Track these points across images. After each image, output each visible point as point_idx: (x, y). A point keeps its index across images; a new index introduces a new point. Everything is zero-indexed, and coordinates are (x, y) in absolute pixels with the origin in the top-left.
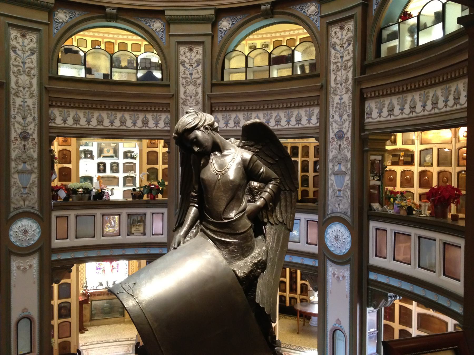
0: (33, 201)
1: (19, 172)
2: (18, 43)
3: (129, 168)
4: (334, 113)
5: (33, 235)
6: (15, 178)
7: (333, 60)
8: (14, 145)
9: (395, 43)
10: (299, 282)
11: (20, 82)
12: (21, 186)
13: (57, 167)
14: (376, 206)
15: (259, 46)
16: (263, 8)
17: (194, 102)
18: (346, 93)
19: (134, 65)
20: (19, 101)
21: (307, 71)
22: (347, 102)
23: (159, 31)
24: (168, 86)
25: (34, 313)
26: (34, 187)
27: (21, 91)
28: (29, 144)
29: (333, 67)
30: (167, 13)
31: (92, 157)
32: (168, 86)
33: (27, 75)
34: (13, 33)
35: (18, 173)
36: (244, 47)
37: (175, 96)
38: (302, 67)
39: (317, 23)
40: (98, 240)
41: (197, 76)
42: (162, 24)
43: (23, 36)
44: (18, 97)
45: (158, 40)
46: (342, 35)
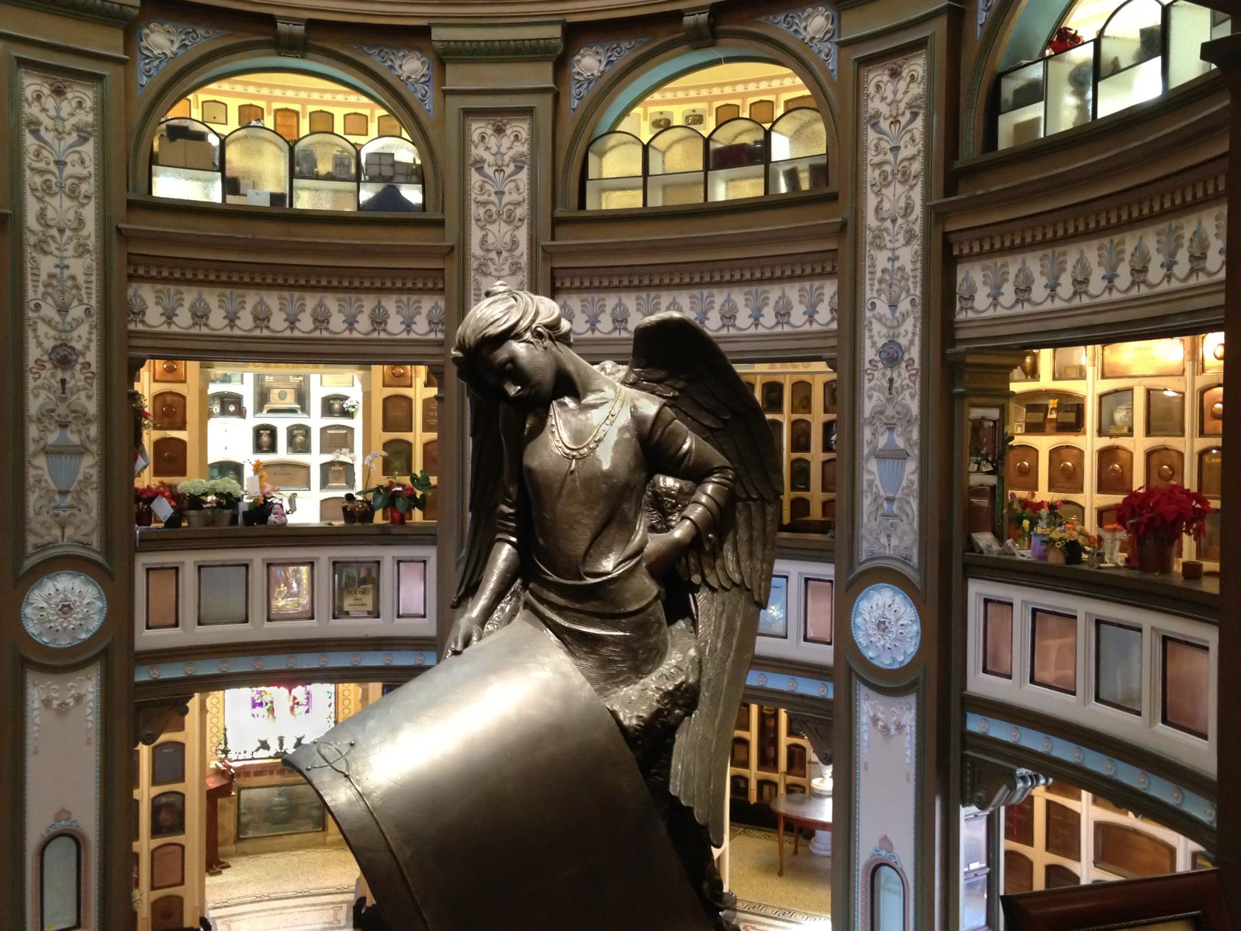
0: (86, 526)
1: (48, 451)
2: (44, 110)
3: (337, 440)
4: (875, 295)
5: (87, 617)
6: (39, 468)
7: (871, 156)
8: (35, 379)
9: (1034, 111)
10: (784, 740)
11: (50, 213)
12: (53, 487)
13: (149, 437)
14: (984, 539)
15: (678, 120)
16: (688, 20)
17: (506, 267)
18: (908, 243)
19: (351, 170)
20: (47, 265)
21: (805, 185)
22: (909, 267)
23: (417, 81)
24: (440, 223)
25: (88, 822)
26: (89, 490)
27: (53, 237)
28: (76, 378)
29: (872, 175)
30: (437, 34)
31: (240, 413)
32: (440, 223)
33: (70, 197)
34: (31, 85)
35: (46, 453)
36: (639, 123)
37: (458, 251)
38: (792, 176)
39: (830, 60)
40: (257, 630)
41: (516, 197)
42: (423, 63)
43: (59, 92)
44: (45, 253)
45: (414, 105)
46: (895, 93)
